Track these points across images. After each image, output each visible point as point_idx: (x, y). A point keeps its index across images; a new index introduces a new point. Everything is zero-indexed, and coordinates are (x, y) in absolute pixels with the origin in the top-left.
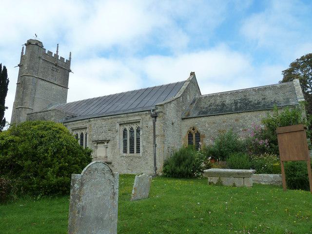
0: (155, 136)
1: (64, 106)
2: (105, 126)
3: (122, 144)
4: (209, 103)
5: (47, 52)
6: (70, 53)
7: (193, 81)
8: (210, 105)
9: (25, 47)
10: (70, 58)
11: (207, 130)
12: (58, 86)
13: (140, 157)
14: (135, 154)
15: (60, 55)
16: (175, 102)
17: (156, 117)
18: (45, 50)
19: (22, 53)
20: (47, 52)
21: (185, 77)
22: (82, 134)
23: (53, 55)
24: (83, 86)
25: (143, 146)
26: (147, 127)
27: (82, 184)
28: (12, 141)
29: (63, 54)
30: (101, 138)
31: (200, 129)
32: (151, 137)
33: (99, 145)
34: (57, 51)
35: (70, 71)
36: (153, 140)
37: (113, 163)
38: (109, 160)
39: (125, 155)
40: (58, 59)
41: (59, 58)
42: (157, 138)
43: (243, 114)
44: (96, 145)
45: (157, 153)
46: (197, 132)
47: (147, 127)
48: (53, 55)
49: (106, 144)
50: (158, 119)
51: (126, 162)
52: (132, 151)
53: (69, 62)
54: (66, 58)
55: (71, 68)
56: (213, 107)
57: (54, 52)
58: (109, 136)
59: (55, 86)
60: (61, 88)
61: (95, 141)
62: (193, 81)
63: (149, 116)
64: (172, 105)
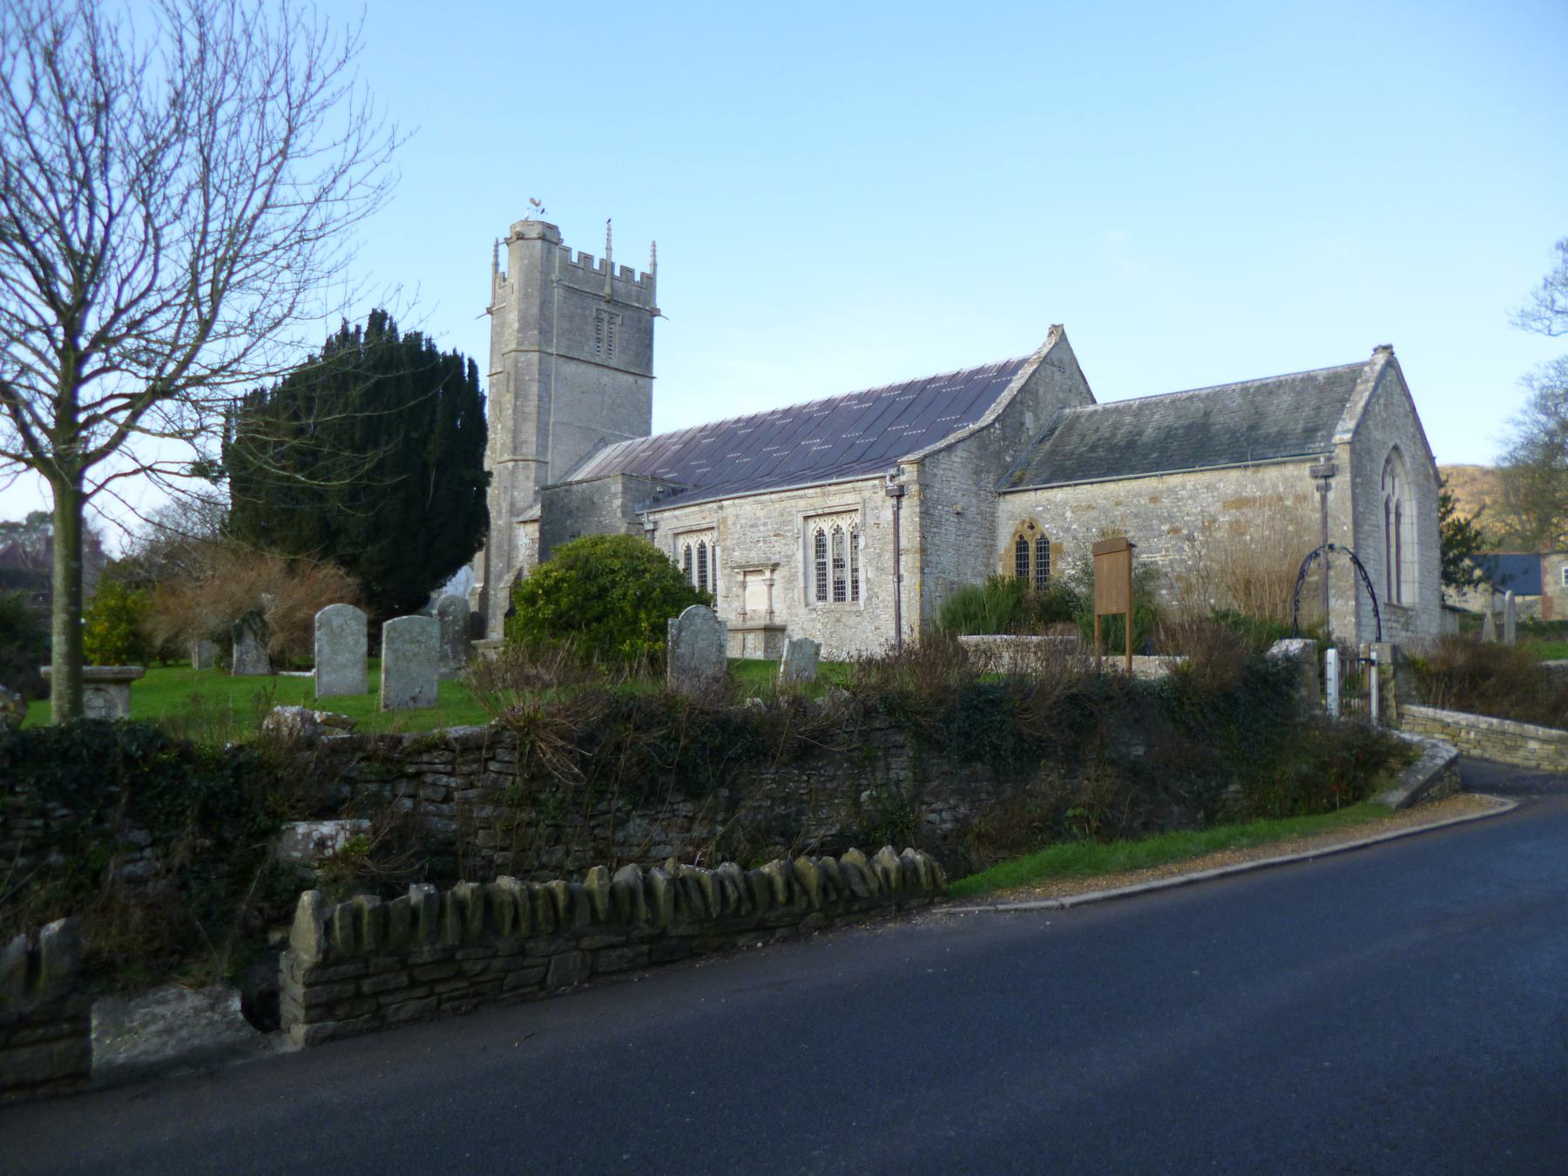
0: (898, 553)
1: (645, 446)
2: (765, 524)
3: (813, 572)
4: (1095, 437)
5: (575, 259)
6: (654, 245)
7: (1059, 360)
8: (1093, 448)
9: (504, 249)
10: (655, 265)
11: (1067, 530)
12: (620, 375)
13: (859, 614)
14: (848, 603)
15: (619, 260)
16: (973, 443)
17: (899, 497)
18: (568, 250)
19: (496, 265)
20: (575, 259)
21: (1028, 344)
22: (702, 546)
23: (596, 266)
24: (697, 387)
25: (868, 580)
26: (878, 525)
27: (680, 630)
28: (563, 580)
29: (631, 257)
30: (755, 556)
31: (1048, 528)
32: (889, 557)
33: (749, 578)
34: (609, 249)
35: (655, 312)
36: (891, 563)
37: (790, 628)
38: (778, 621)
39: (820, 603)
40: (613, 277)
41: (617, 273)
42: (903, 558)
43: (1174, 480)
44: (740, 578)
45: (904, 598)
46: (1043, 536)
47: (878, 525)
48: (596, 266)
49: (768, 574)
50: (905, 502)
51: (825, 625)
52: (840, 595)
53: (649, 281)
54: (641, 267)
55: (661, 301)
56: (1101, 452)
57: (598, 254)
58: (778, 549)
59: (612, 373)
60: (631, 379)
61: (739, 567)
62: (1059, 360)
63: (883, 493)
64: (959, 456)
